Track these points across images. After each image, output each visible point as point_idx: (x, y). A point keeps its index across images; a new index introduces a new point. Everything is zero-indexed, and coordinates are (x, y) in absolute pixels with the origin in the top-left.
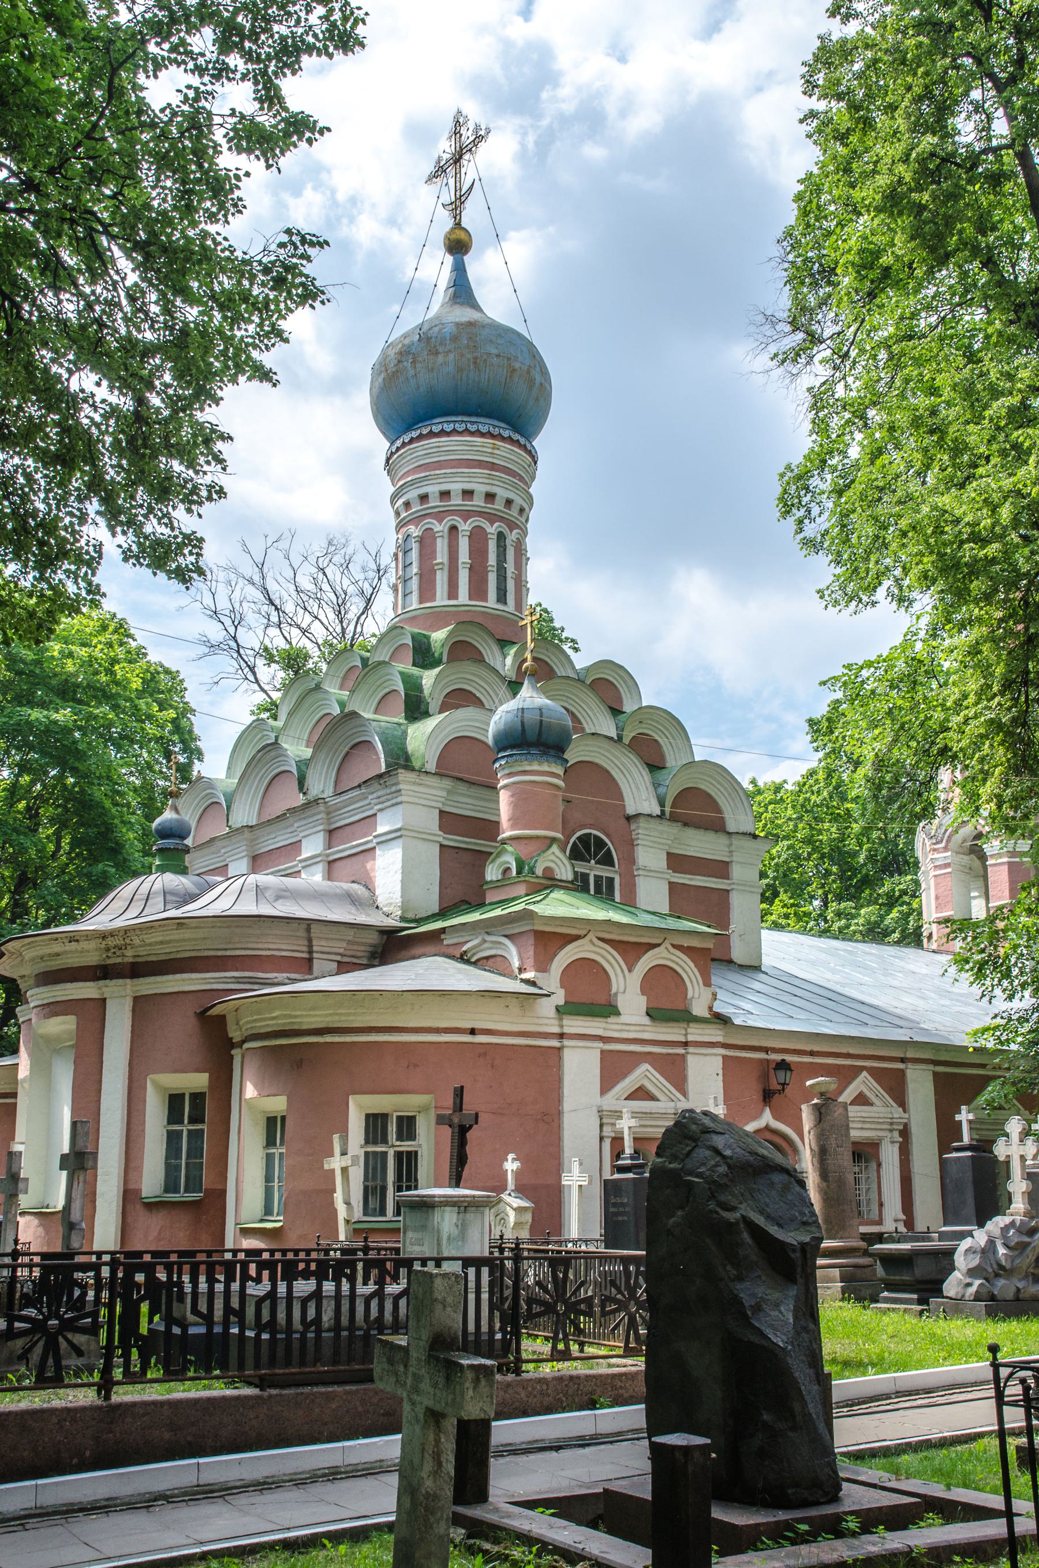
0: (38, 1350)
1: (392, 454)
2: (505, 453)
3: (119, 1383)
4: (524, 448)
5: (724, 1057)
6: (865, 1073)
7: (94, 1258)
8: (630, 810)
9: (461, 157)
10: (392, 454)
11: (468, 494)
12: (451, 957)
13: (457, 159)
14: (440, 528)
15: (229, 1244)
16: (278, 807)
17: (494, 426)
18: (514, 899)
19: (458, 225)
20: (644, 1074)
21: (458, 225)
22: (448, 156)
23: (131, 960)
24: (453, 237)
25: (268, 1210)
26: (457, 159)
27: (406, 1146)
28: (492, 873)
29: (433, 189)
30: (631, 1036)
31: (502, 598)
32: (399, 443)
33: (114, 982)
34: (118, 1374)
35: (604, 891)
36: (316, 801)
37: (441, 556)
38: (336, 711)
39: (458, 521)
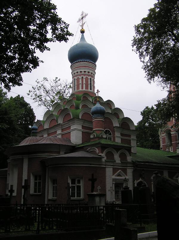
1: (72, 65)
2: (91, 65)
3: (41, 230)
4: (94, 64)
6: (178, 173)
7: (55, 205)
8: (114, 126)
10: (72, 65)
12: (85, 151)
13: (82, 18)
14: (80, 77)
15: (46, 203)
16: (52, 126)
18: (96, 141)
19: (82, 28)
21: (82, 28)
26: (82, 18)
28: (92, 137)
29: (78, 23)
31: (91, 89)
32: (73, 63)
34: (40, 229)
35: (110, 139)
36: (60, 124)
37: (81, 82)
38: (63, 109)
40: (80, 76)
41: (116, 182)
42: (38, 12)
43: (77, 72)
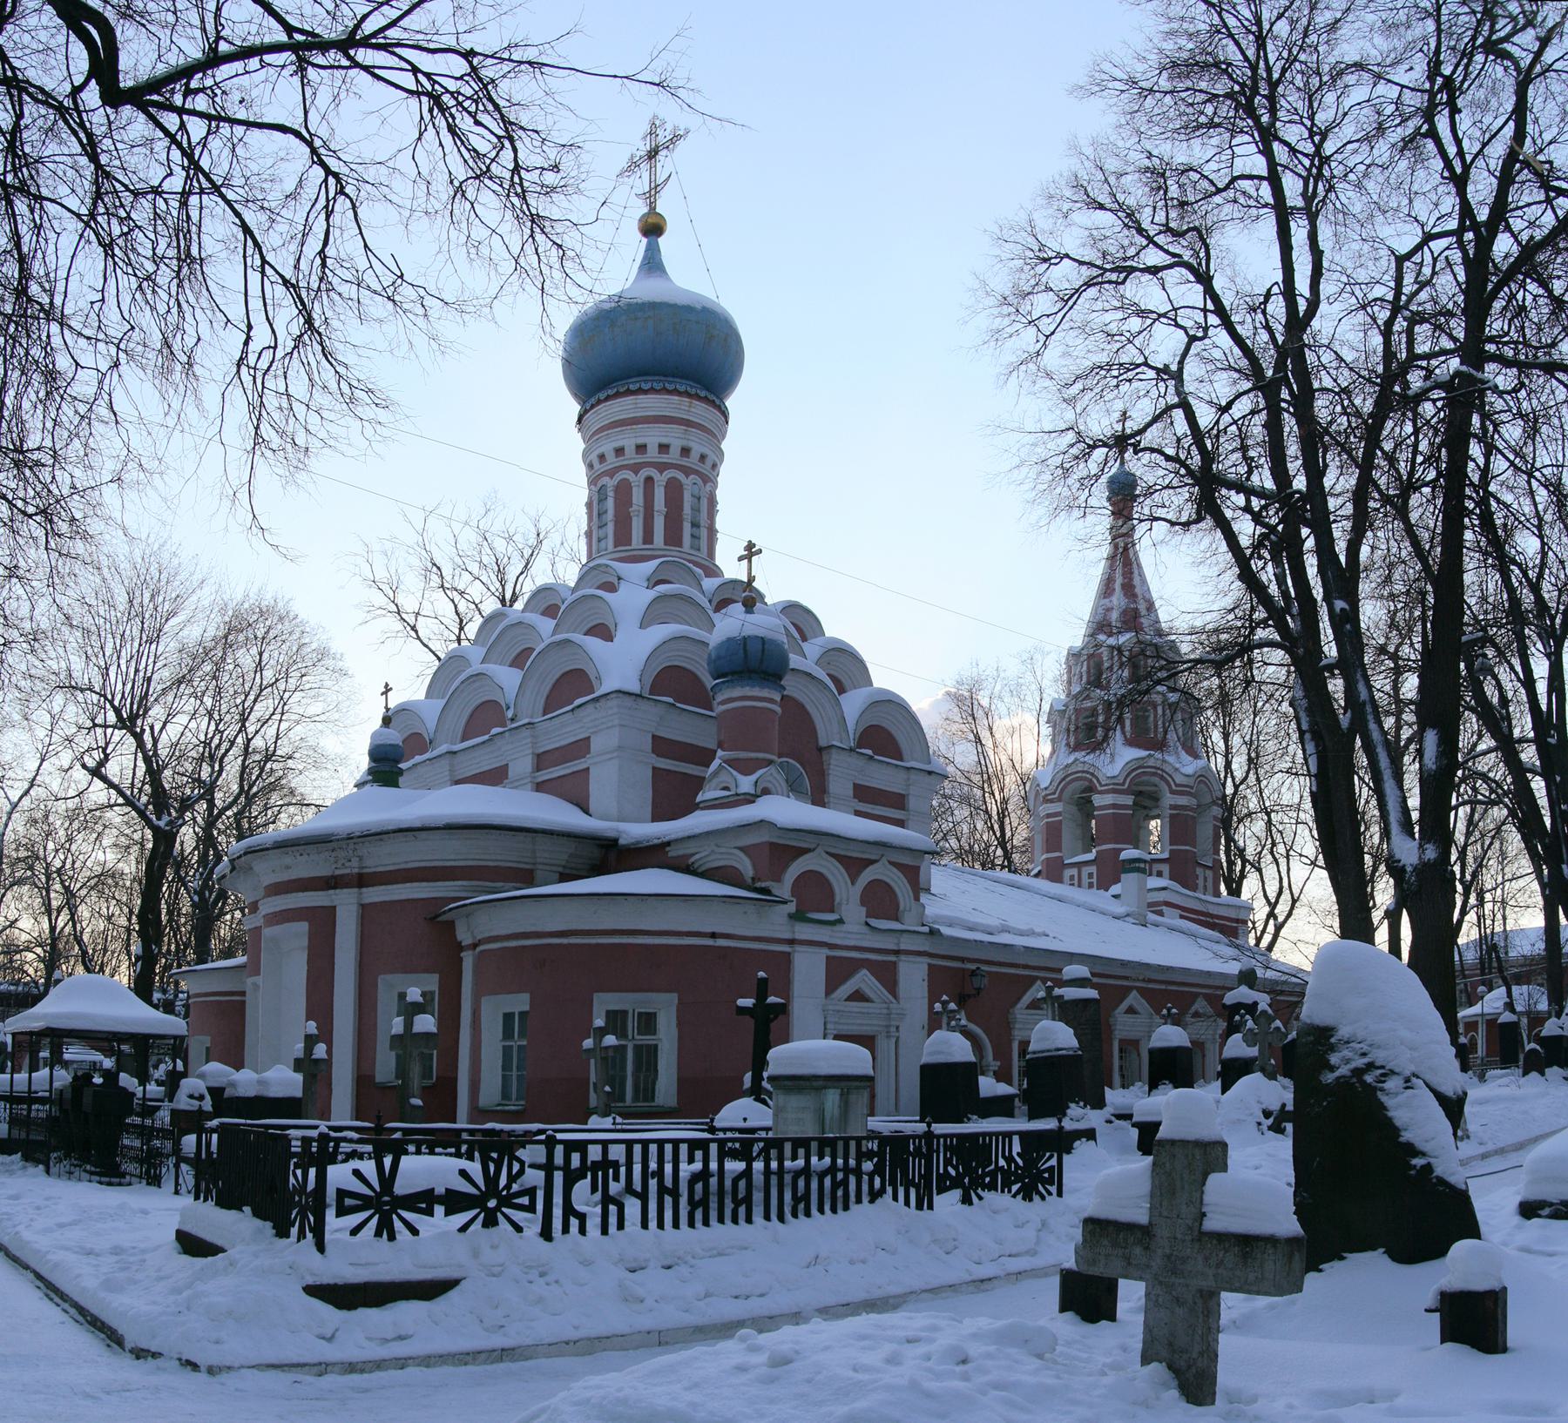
0: (503, 1181)
2: (699, 411)
5: (929, 965)
9: (656, 153)
11: (664, 448)
13: (652, 154)
17: (691, 387)
19: (652, 208)
20: (864, 980)
22: (643, 153)
23: (356, 871)
24: (650, 220)
25: (505, 1094)
26: (652, 154)
27: (646, 1039)
30: (852, 943)
33: (345, 890)
39: (653, 472)
40: (661, 473)
41: (841, 1027)
42: (1434, 607)
43: (619, 451)
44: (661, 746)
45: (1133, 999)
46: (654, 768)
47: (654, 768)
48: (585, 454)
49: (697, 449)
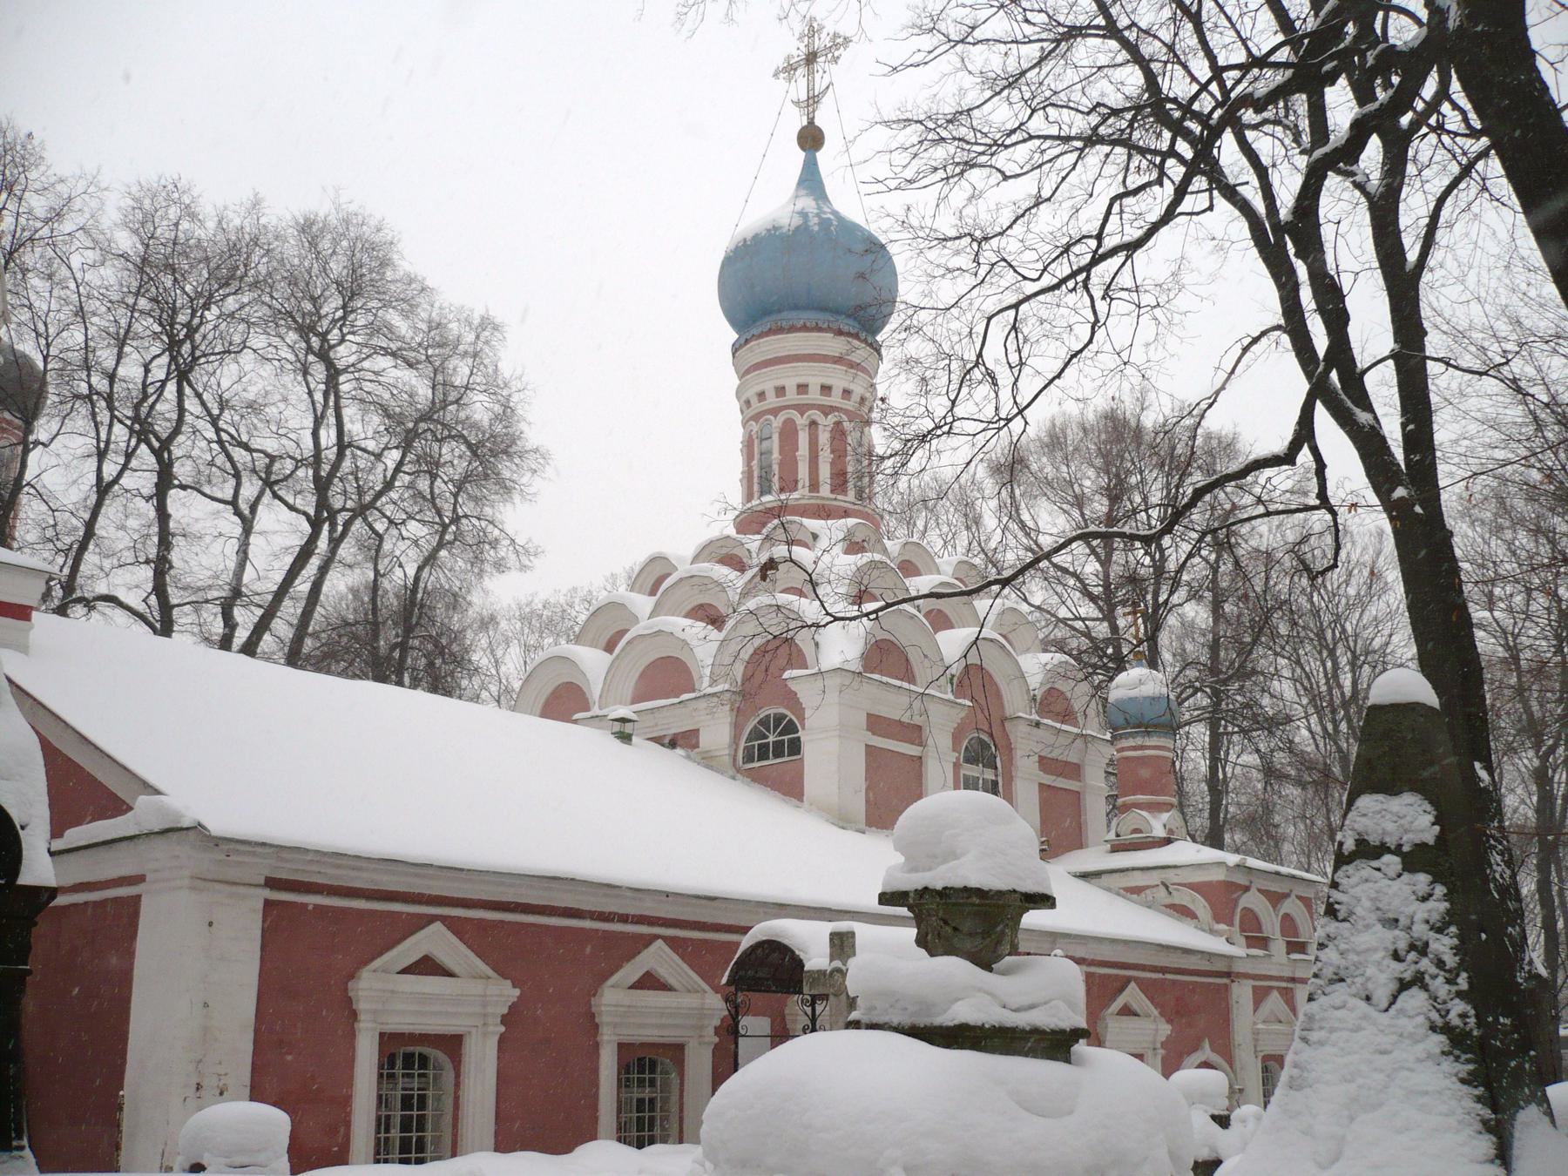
13: (811, 58)
26: (811, 58)
39: (794, 414)
40: (826, 415)
43: (761, 395)
44: (876, 724)
45: (1132, 995)
46: (867, 746)
47: (867, 746)
48: (739, 393)
49: (858, 389)
